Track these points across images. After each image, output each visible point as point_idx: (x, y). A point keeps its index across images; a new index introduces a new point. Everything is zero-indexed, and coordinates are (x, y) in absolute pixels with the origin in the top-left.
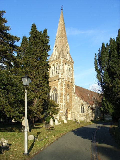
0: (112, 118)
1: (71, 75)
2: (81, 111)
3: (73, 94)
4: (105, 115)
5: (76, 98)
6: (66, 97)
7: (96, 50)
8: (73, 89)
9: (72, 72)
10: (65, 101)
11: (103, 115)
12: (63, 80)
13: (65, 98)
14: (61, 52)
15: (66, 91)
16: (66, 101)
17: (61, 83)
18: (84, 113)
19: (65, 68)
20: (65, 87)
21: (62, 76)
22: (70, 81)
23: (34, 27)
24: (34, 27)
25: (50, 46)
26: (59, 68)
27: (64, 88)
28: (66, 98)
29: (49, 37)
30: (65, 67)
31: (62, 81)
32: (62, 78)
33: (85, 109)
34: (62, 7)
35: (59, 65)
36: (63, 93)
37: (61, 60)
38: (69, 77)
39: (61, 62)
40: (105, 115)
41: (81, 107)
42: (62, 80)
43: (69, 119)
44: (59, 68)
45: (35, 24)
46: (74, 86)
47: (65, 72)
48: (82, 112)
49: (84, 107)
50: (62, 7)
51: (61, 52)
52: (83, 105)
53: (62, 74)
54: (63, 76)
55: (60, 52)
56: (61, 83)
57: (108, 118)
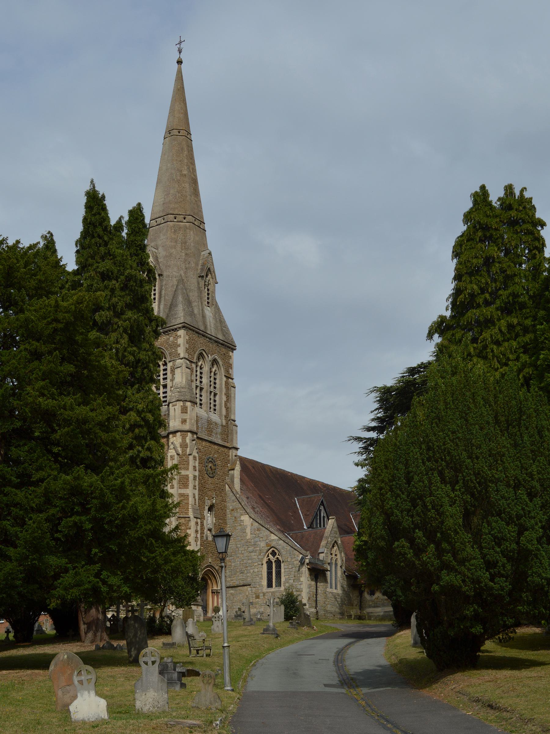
0: (391, 609)
1: (224, 410)
2: (265, 582)
3: (231, 504)
4: (366, 596)
5: (246, 519)
6: (202, 518)
7: (451, 243)
8: (233, 475)
9: (228, 396)
10: (199, 536)
11: (361, 594)
12: (188, 440)
13: (197, 523)
14: (180, 298)
15: (202, 490)
16: (202, 537)
17: (180, 452)
18: (277, 589)
19: (198, 378)
20: (197, 473)
21: (184, 421)
22: (220, 442)
23: (95, 203)
24: (95, 203)
25: (430, 336)
26: (172, 380)
27: (195, 477)
28: (202, 525)
29: (31, 245)
30: (198, 373)
31: (184, 445)
32: (187, 427)
33: (282, 570)
34: (180, 51)
35: (169, 365)
36: (191, 500)
37: (180, 341)
38: (215, 417)
39: (181, 351)
40: (366, 596)
41: (265, 560)
42: (184, 439)
43: (108, 468)
44: (169, 376)
45: (101, 189)
46: (234, 464)
47: (198, 396)
48: (270, 585)
49: (278, 562)
50: (180, 51)
51: (180, 298)
52: (273, 553)
53: (184, 410)
54: (191, 419)
55: (175, 296)
56: (180, 450)
57: (379, 610)
